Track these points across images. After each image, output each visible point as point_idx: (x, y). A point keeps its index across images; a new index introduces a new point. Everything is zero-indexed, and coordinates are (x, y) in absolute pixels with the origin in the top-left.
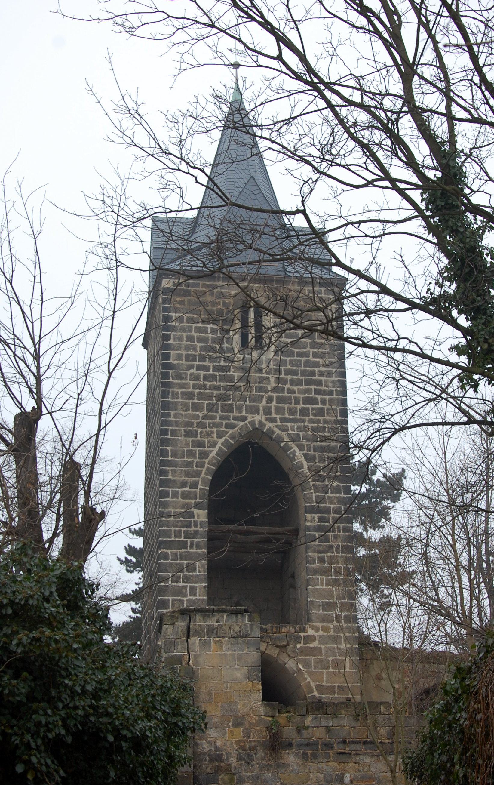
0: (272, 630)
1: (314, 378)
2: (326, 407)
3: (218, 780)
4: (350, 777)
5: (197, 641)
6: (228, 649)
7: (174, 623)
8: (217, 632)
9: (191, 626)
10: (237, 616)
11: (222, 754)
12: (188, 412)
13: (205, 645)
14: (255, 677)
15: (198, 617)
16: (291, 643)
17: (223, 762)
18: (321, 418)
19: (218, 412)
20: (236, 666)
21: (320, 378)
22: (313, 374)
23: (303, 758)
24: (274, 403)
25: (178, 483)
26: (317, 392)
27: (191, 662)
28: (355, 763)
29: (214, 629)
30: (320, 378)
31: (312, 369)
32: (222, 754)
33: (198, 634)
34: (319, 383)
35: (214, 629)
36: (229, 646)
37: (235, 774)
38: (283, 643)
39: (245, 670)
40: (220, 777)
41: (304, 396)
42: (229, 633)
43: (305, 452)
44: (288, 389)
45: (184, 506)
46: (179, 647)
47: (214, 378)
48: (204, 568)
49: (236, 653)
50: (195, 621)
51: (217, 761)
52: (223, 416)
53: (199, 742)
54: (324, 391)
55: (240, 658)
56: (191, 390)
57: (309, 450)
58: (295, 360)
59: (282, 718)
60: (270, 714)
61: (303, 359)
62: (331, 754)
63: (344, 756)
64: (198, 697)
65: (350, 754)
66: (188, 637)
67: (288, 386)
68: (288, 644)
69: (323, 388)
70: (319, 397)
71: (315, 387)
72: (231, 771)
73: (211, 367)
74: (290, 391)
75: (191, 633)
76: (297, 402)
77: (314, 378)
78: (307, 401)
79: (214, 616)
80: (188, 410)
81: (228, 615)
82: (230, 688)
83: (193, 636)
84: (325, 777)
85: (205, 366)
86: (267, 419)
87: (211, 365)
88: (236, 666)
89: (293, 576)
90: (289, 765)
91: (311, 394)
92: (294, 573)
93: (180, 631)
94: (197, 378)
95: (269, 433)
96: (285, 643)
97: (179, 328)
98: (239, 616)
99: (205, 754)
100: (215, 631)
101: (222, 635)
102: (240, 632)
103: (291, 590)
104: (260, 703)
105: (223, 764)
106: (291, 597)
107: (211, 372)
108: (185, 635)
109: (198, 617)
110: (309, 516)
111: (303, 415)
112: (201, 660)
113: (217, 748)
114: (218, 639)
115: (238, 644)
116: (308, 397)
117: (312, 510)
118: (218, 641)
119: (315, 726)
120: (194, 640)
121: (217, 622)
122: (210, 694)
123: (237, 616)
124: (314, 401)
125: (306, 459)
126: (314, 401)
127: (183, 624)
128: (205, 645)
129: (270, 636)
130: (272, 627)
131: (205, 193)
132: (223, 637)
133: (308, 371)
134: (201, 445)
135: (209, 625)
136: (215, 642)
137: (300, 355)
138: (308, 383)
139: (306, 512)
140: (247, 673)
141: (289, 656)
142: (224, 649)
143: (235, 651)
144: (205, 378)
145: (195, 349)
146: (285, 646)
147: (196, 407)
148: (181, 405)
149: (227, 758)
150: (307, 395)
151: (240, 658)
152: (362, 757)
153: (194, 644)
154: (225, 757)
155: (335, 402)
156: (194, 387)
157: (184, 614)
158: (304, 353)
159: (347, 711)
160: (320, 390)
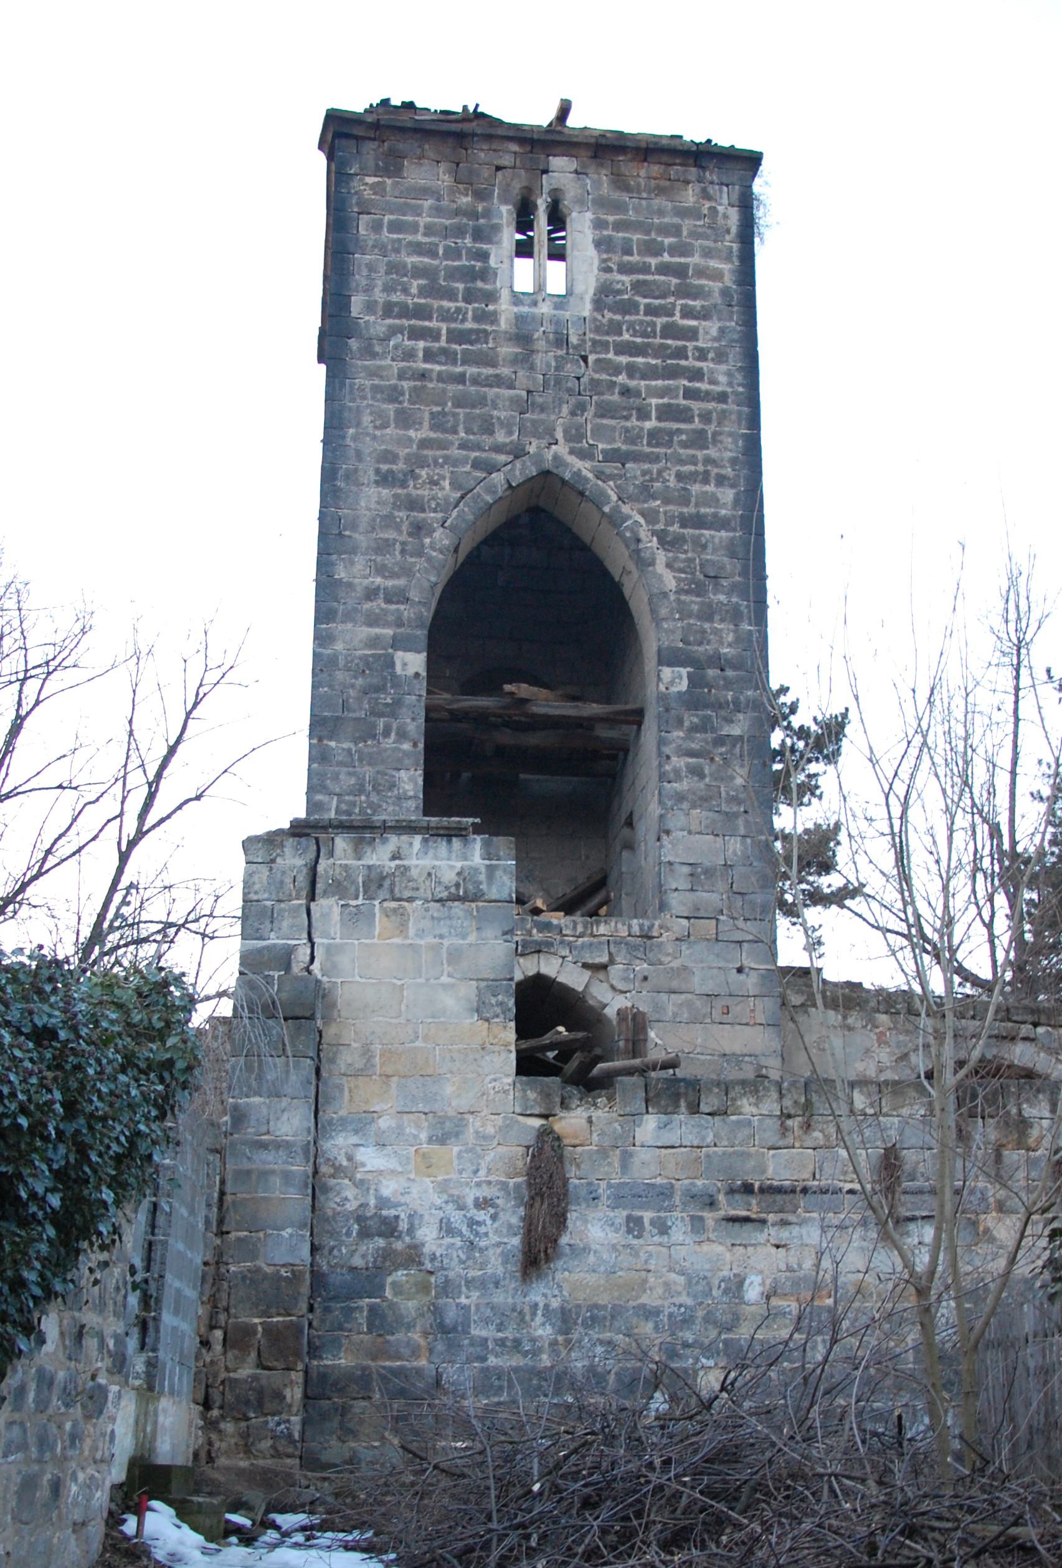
0: (575, 928)
1: (683, 363)
2: (711, 428)
3: (382, 1287)
4: (763, 1284)
5: (337, 910)
6: (421, 933)
7: (273, 861)
8: (393, 884)
9: (320, 868)
10: (449, 842)
11: (397, 1217)
12: (388, 431)
13: (356, 919)
14: (498, 1010)
15: (342, 843)
16: (618, 959)
17: (399, 1237)
18: (700, 454)
19: (456, 432)
20: (445, 979)
21: (699, 364)
22: (681, 353)
23: (629, 1231)
24: (589, 414)
25: (359, 589)
26: (689, 394)
27: (316, 967)
28: (778, 1247)
29: (383, 878)
30: (699, 364)
31: (680, 343)
32: (397, 1217)
33: (339, 888)
34: (697, 375)
35: (383, 878)
36: (426, 924)
37: (431, 1273)
38: (597, 960)
39: (469, 990)
40: (390, 1279)
41: (661, 401)
42: (425, 891)
43: (660, 526)
44: (622, 385)
45: (374, 642)
46: (285, 924)
47: (449, 356)
48: (416, 784)
49: (446, 942)
50: (331, 854)
51: (381, 1234)
52: (468, 441)
53: (332, 1182)
54: (707, 393)
55: (455, 956)
56: (393, 382)
57: (669, 522)
58: (641, 322)
59: (573, 1121)
60: (537, 1111)
61: (660, 321)
62: (710, 1223)
63: (748, 1227)
64: (332, 1061)
65: (764, 1222)
66: (312, 897)
67: (622, 379)
68: (612, 961)
69: (704, 386)
70: (696, 406)
71: (686, 382)
72: (421, 1263)
73: (444, 332)
74: (626, 392)
75: (320, 886)
76: (644, 415)
77: (683, 363)
78: (666, 413)
79: (385, 841)
80: (384, 426)
81: (425, 841)
82: (426, 1038)
83: (325, 893)
84: (689, 1283)
85: (430, 329)
86: (572, 452)
87: (444, 327)
88: (445, 979)
89: (630, 823)
90: (586, 1249)
91: (677, 397)
92: (631, 814)
93: (288, 880)
94: (410, 355)
95: (576, 490)
96: (604, 959)
97: (370, 243)
98: (456, 843)
99: (347, 1216)
100: (387, 883)
101: (407, 894)
102: (457, 885)
103: (625, 854)
104: (510, 1080)
105: (399, 1246)
106: (624, 869)
107: (443, 343)
108: (304, 893)
109: (342, 843)
110: (667, 672)
111: (658, 445)
112: (344, 961)
113: (383, 1203)
114: (394, 904)
115: (450, 918)
116: (669, 405)
117: (670, 658)
118: (395, 910)
119: (657, 1141)
120: (328, 907)
121: (394, 858)
122: (366, 1051)
123: (449, 842)
124: (684, 415)
125: (662, 542)
126: (684, 415)
127: (299, 862)
128: (356, 919)
129: (570, 944)
130: (575, 924)
131: (512, 277)
132: (410, 900)
133: (668, 347)
134: (414, 504)
135: (369, 867)
136: (386, 914)
137: (650, 311)
138: (673, 373)
139: (661, 662)
140: (474, 998)
141: (613, 987)
142: (412, 932)
143: (441, 937)
144: (429, 356)
145: (405, 291)
146: (604, 967)
147: (405, 420)
148: (371, 414)
149: (411, 1231)
150: (665, 400)
151: (455, 956)
152: (796, 1230)
153: (326, 916)
154: (403, 1226)
155: (733, 417)
156: (401, 376)
157: (300, 835)
158: (661, 307)
159: (756, 1105)
160: (698, 390)
